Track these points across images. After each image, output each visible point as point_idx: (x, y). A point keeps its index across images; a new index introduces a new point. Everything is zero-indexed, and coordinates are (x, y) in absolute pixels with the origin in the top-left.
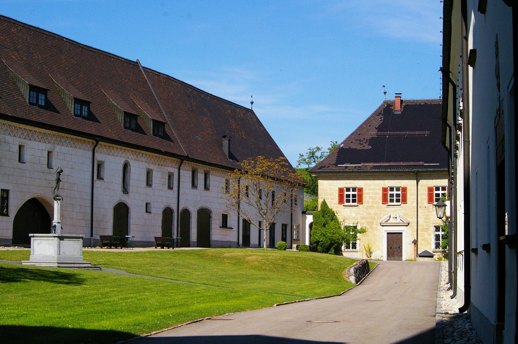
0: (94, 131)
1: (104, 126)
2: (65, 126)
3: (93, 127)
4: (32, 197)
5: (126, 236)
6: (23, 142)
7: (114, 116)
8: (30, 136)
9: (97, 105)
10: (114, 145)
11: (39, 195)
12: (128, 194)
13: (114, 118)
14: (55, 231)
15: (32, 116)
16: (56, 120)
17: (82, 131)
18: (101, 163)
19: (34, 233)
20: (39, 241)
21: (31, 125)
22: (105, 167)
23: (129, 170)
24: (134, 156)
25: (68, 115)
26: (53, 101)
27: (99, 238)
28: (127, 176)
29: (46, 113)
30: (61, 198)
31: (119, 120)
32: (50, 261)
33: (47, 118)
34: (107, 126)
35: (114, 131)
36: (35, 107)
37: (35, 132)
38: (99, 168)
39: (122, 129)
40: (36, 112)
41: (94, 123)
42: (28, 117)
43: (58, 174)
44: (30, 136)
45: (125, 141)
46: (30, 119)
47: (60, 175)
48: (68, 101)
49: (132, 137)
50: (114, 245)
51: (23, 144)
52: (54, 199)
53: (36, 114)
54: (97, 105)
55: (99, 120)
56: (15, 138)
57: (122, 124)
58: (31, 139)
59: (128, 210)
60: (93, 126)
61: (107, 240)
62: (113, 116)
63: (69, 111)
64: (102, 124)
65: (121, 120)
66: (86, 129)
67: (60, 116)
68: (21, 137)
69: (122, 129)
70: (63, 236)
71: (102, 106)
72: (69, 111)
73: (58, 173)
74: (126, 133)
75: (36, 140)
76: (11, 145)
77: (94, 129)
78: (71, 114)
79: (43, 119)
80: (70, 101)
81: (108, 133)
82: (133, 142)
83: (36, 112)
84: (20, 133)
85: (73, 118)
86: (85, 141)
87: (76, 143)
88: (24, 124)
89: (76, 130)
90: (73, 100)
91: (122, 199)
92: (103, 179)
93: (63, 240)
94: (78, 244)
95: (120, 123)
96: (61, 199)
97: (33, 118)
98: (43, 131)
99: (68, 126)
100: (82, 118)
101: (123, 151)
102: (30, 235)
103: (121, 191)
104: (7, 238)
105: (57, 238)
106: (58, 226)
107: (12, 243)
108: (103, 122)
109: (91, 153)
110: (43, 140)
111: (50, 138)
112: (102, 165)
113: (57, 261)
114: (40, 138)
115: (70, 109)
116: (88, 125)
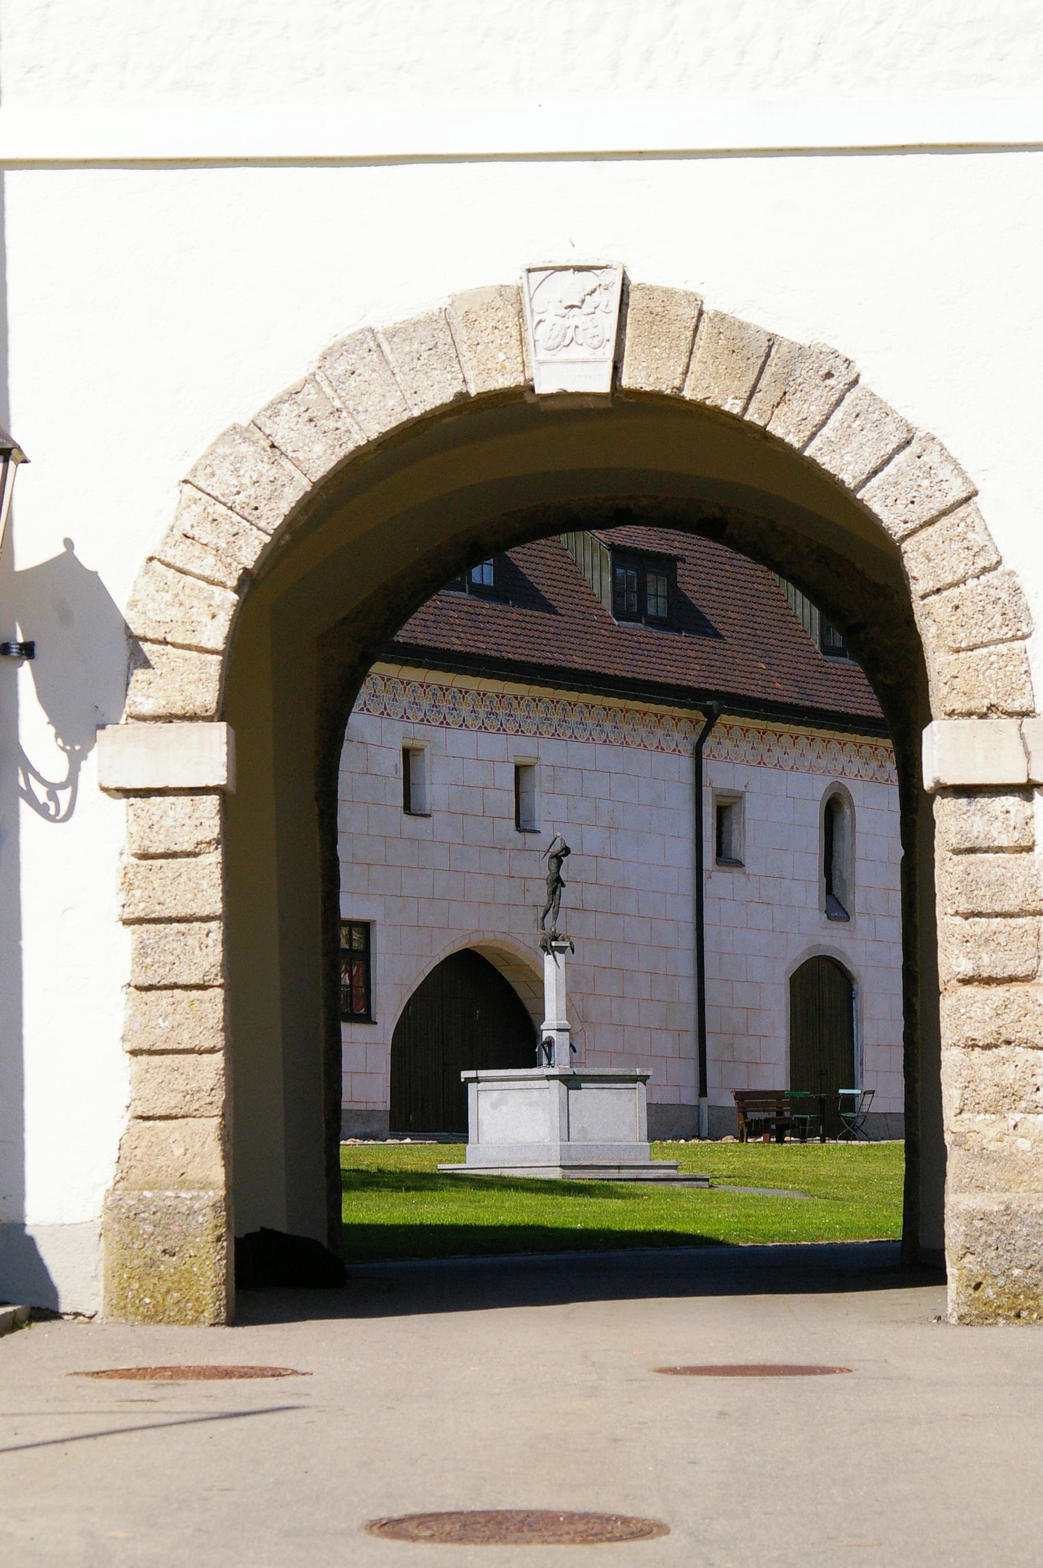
0: (695, 673)
1: (738, 648)
2: (578, 662)
3: (690, 660)
4: (459, 946)
5: (841, 1091)
6: (418, 734)
7: (780, 604)
8: (445, 710)
9: (705, 563)
10: (779, 726)
11: (489, 936)
12: (847, 918)
13: (783, 611)
14: (549, 1058)
15: (450, 633)
16: (545, 642)
17: (646, 678)
18: (730, 800)
19: (477, 1069)
20: (495, 1094)
21: (447, 670)
22: (748, 815)
23: (847, 822)
24: (866, 763)
25: (591, 617)
26: (528, 565)
27: (730, 1102)
28: (841, 847)
29: (502, 615)
30: (568, 944)
31: (801, 621)
32: (537, 1161)
33: (509, 636)
34: (749, 650)
35: (780, 669)
36: (456, 594)
37: (461, 692)
38: (725, 822)
39: (814, 656)
40: (463, 615)
41: (695, 641)
42: (435, 638)
43: (555, 860)
44: (445, 710)
45: (827, 707)
46: (442, 646)
47: (560, 862)
48: (588, 559)
49: (858, 687)
50: (793, 1126)
51: (417, 744)
52: (544, 948)
53: (464, 622)
54: (705, 563)
55: (715, 625)
56: (386, 722)
57: (814, 637)
58: (448, 724)
59: (852, 990)
60: (693, 654)
61: (765, 1107)
62: (775, 603)
63: (592, 598)
64: (730, 640)
65: (807, 621)
66: (662, 667)
67: (557, 624)
68: (408, 718)
69: (814, 656)
70: (577, 1073)
71: (727, 567)
72: (592, 598)
73: (552, 857)
74: (829, 670)
75: (467, 726)
76: (372, 749)
77: (697, 667)
78: (600, 613)
79: (493, 640)
80: (597, 560)
81: (753, 676)
82: (861, 706)
83: (463, 615)
84: (404, 701)
85: (611, 628)
86: (662, 717)
87: (626, 728)
88: (419, 665)
89: (624, 674)
90: (609, 553)
91: (825, 941)
92: (739, 864)
93: (581, 1089)
94: (630, 1100)
95: (803, 634)
96: (569, 948)
97: (454, 640)
98: (492, 686)
99: (592, 662)
100: (647, 624)
101: (818, 745)
102: (465, 1074)
103: (817, 912)
104: (370, 1107)
105: (558, 1081)
106: (561, 1042)
107: (387, 1127)
108: (734, 635)
109: (686, 764)
110: (513, 726)
111: (519, 714)
112: (735, 809)
113: (561, 1159)
114: (482, 715)
115: (596, 591)
116: (671, 651)
